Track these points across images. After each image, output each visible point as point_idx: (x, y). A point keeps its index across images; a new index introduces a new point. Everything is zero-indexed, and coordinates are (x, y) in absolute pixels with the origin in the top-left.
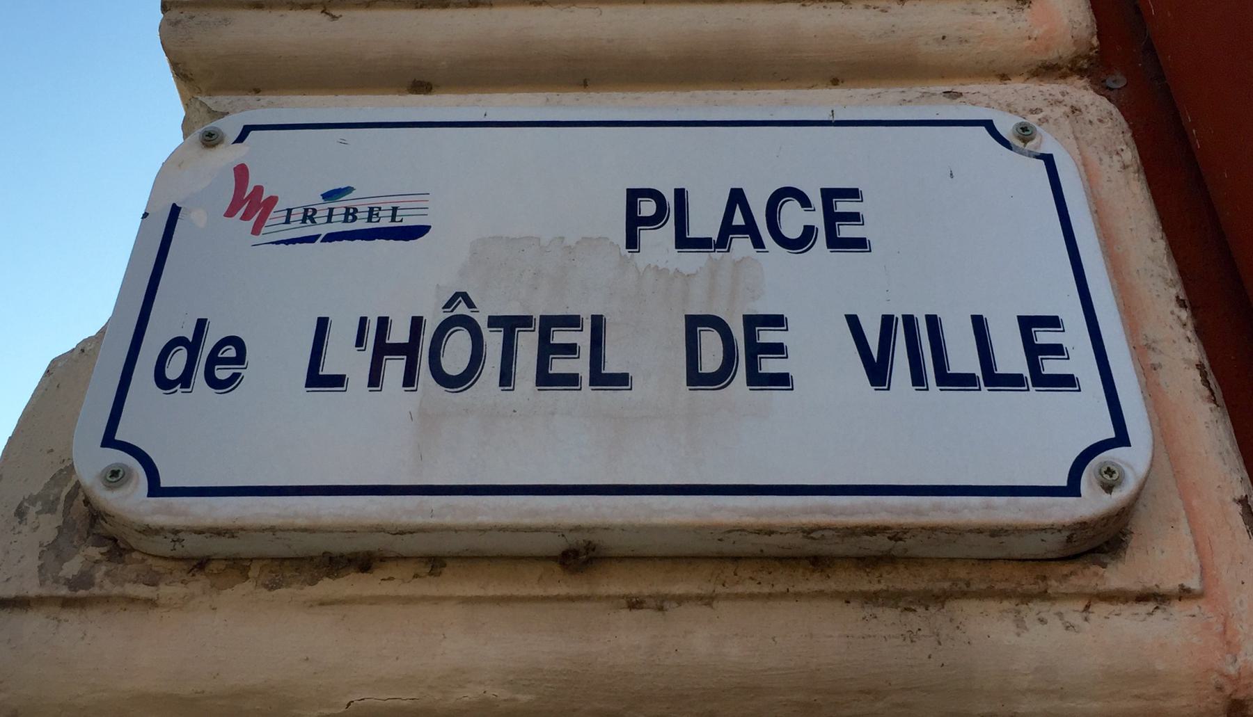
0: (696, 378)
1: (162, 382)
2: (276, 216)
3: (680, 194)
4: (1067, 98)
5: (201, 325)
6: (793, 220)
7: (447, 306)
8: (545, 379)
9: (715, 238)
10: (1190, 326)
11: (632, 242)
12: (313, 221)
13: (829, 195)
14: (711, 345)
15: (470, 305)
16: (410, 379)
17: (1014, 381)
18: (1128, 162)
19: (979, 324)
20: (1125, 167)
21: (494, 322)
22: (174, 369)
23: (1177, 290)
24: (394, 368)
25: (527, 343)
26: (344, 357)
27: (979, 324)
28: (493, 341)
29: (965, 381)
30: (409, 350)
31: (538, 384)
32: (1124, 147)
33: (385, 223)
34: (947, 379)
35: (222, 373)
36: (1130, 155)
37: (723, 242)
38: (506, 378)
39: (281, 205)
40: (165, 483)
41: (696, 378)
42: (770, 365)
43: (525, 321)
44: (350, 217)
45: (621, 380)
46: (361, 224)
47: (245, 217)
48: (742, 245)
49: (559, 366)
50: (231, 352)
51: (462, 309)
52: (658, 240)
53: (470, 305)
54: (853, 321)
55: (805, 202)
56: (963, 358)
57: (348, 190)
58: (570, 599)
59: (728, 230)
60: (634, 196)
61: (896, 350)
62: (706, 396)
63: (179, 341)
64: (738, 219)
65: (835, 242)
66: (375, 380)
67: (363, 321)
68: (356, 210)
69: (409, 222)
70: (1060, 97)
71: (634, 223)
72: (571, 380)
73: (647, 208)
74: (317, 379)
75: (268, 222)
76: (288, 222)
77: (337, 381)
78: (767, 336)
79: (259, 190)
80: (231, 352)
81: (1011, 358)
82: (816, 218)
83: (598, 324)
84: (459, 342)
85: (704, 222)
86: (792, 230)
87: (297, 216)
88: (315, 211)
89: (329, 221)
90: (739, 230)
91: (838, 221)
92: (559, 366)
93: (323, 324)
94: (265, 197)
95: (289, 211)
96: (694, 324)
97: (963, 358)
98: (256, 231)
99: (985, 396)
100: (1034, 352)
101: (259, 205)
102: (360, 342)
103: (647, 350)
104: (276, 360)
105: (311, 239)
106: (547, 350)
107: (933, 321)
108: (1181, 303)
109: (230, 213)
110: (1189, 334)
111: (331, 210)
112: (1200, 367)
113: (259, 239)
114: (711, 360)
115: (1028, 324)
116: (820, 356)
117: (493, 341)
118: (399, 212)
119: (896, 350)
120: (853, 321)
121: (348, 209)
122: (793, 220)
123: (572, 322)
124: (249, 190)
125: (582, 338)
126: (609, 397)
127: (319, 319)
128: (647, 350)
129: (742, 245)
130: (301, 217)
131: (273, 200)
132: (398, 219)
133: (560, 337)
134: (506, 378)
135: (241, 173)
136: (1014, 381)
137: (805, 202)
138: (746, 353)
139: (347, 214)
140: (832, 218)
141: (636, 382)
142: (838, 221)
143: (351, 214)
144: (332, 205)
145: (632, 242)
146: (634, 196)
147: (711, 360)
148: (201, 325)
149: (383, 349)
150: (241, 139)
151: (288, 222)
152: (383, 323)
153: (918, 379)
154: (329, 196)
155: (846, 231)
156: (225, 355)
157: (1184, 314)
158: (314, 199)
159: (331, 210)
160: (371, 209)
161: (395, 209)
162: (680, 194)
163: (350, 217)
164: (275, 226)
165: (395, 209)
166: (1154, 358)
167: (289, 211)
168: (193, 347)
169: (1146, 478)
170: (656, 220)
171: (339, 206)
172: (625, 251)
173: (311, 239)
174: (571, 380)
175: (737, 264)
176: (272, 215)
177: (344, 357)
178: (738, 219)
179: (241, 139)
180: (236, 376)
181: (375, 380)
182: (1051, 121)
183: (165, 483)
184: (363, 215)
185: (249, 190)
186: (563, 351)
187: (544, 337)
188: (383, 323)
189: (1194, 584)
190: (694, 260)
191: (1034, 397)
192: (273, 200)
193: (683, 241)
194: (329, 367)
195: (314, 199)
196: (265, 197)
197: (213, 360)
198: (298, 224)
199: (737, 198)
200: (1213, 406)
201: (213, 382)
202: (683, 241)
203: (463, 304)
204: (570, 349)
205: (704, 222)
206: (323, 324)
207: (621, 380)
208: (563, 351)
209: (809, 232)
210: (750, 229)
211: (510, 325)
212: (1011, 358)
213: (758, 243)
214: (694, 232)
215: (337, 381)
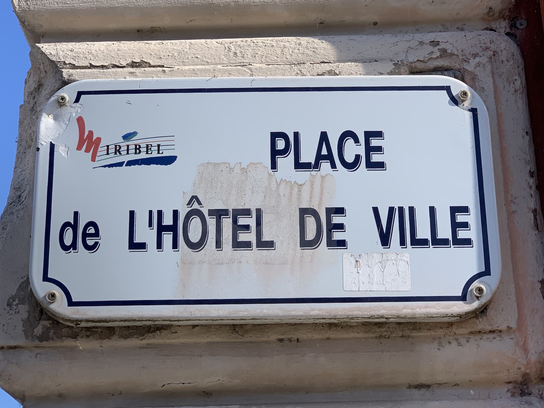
0: (305, 244)
1: (65, 248)
2: (102, 150)
3: (296, 135)
4: (492, 46)
5: (76, 214)
6: (352, 150)
7: (189, 204)
8: (237, 245)
9: (313, 163)
10: (534, 187)
11: (274, 166)
12: (120, 154)
13: (369, 135)
14: (310, 222)
15: (200, 203)
16: (175, 245)
17: (444, 242)
18: (517, 88)
19: (432, 210)
20: (516, 91)
21: (212, 212)
22: (68, 241)
23: (532, 167)
24: (167, 238)
25: (227, 223)
26: (146, 234)
27: (432, 210)
28: (211, 222)
29: (423, 242)
30: (173, 228)
31: (233, 247)
32: (517, 77)
33: (155, 155)
34: (417, 242)
35: (90, 242)
36: (519, 82)
37: (317, 165)
38: (219, 244)
39: (103, 143)
40: (74, 300)
41: (305, 244)
42: (337, 236)
43: (225, 212)
44: (138, 151)
45: (270, 245)
46: (143, 156)
47: (87, 151)
48: (325, 165)
49: (243, 237)
50: (92, 230)
51: (196, 206)
52: (286, 163)
53: (200, 203)
54: (376, 210)
55: (357, 141)
56: (424, 232)
57: (134, 134)
58: (179, 321)
59: (319, 157)
60: (274, 136)
61: (395, 227)
62: (308, 252)
63: (66, 225)
64: (324, 152)
65: (371, 165)
66: (159, 245)
67: (151, 212)
68: (140, 146)
69: (166, 154)
70: (489, 45)
71: (275, 153)
72: (247, 245)
73: (281, 144)
74: (136, 246)
75: (98, 154)
76: (108, 154)
77: (142, 246)
78: (337, 219)
79: (91, 133)
80: (92, 230)
81: (444, 231)
82: (361, 150)
83: (259, 212)
84: (195, 224)
85: (308, 155)
86: (349, 158)
87: (112, 150)
88: (120, 147)
89: (128, 153)
90: (325, 158)
91: (371, 152)
92: (243, 237)
93: (132, 213)
94: (94, 138)
95: (108, 146)
96: (304, 212)
97: (423, 232)
98: (93, 159)
99: (431, 251)
100: (456, 226)
101: (93, 143)
102: (150, 225)
103: (281, 228)
104: (113, 235)
105: (120, 164)
106: (237, 228)
107: (412, 209)
108: (531, 174)
109: (79, 148)
110: (532, 192)
111: (128, 146)
112: (535, 211)
113: (96, 164)
114: (310, 235)
115: (455, 210)
116: (359, 228)
117: (211, 222)
118: (161, 148)
119: (395, 227)
120: (376, 210)
121: (136, 146)
122: (352, 150)
123: (247, 212)
124: (86, 133)
125: (251, 222)
126: (265, 253)
127: (130, 211)
128: (281, 228)
129: (325, 165)
130: (114, 150)
131: (99, 140)
132: (161, 152)
133: (242, 221)
134: (219, 244)
135: (80, 121)
136: (444, 242)
137: (357, 141)
138: (325, 229)
139: (136, 149)
140: (369, 149)
141: (277, 244)
142: (371, 152)
143: (138, 149)
144: (128, 143)
145: (274, 166)
146: (274, 136)
147: (310, 235)
148: (76, 214)
149: (161, 229)
150: (77, 100)
151: (108, 154)
152: (160, 213)
153: (403, 242)
154: (127, 137)
155: (376, 158)
156: (90, 232)
157: (531, 181)
158: (119, 139)
159: (128, 146)
160: (147, 145)
161: (159, 146)
162: (296, 135)
163: (138, 151)
164: (103, 159)
165: (159, 146)
166: (513, 207)
167: (108, 146)
168: (75, 227)
169: (496, 292)
170: (284, 152)
171: (132, 143)
172: (271, 171)
173: (120, 164)
174: (247, 245)
175: (322, 177)
176: (100, 149)
177: (146, 234)
178: (324, 152)
179: (77, 100)
180: (96, 243)
181: (159, 245)
182: (481, 65)
183: (74, 300)
184: (144, 150)
185: (86, 133)
186: (242, 227)
187: (235, 221)
188: (160, 213)
189: (513, 325)
190: (304, 175)
191: (453, 251)
192: (99, 140)
193: (299, 165)
194: (138, 239)
195: (119, 139)
196: (94, 138)
197: (85, 235)
198: (113, 155)
199: (324, 137)
200: (537, 232)
201: (89, 248)
202: (299, 165)
203: (196, 203)
204: (247, 227)
205: (308, 155)
206: (132, 213)
207: (270, 245)
208: (242, 227)
209: (358, 157)
210: (329, 157)
211: (219, 214)
212: (444, 231)
213: (333, 166)
214: (303, 160)
215: (142, 246)
